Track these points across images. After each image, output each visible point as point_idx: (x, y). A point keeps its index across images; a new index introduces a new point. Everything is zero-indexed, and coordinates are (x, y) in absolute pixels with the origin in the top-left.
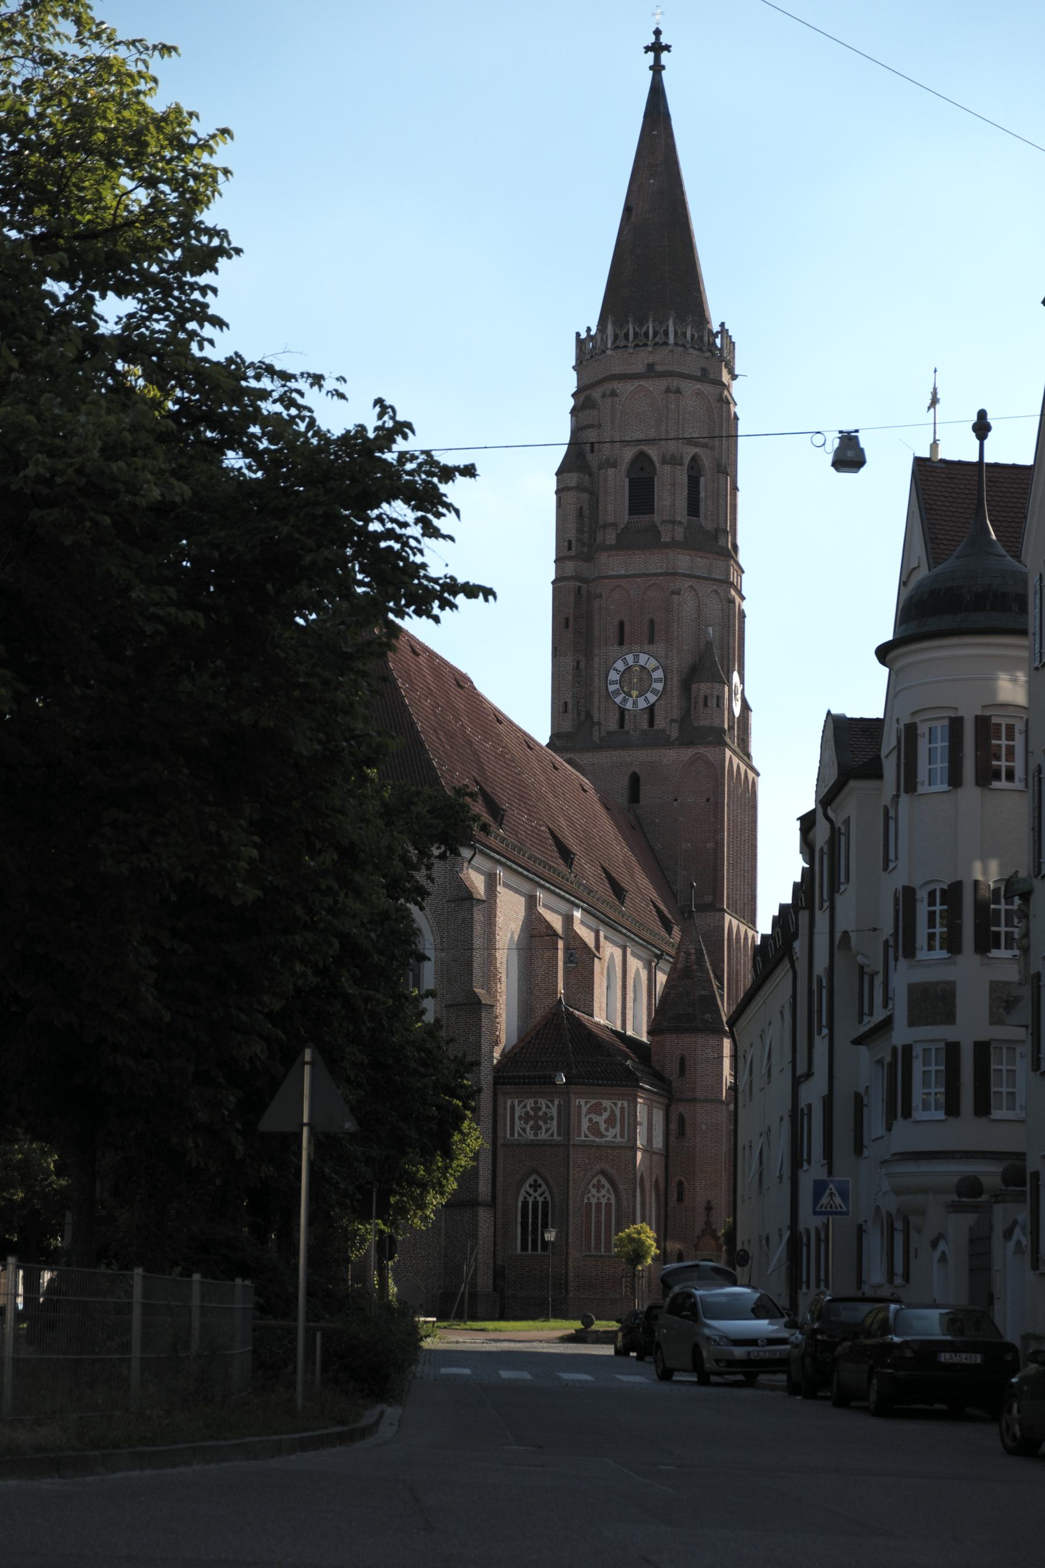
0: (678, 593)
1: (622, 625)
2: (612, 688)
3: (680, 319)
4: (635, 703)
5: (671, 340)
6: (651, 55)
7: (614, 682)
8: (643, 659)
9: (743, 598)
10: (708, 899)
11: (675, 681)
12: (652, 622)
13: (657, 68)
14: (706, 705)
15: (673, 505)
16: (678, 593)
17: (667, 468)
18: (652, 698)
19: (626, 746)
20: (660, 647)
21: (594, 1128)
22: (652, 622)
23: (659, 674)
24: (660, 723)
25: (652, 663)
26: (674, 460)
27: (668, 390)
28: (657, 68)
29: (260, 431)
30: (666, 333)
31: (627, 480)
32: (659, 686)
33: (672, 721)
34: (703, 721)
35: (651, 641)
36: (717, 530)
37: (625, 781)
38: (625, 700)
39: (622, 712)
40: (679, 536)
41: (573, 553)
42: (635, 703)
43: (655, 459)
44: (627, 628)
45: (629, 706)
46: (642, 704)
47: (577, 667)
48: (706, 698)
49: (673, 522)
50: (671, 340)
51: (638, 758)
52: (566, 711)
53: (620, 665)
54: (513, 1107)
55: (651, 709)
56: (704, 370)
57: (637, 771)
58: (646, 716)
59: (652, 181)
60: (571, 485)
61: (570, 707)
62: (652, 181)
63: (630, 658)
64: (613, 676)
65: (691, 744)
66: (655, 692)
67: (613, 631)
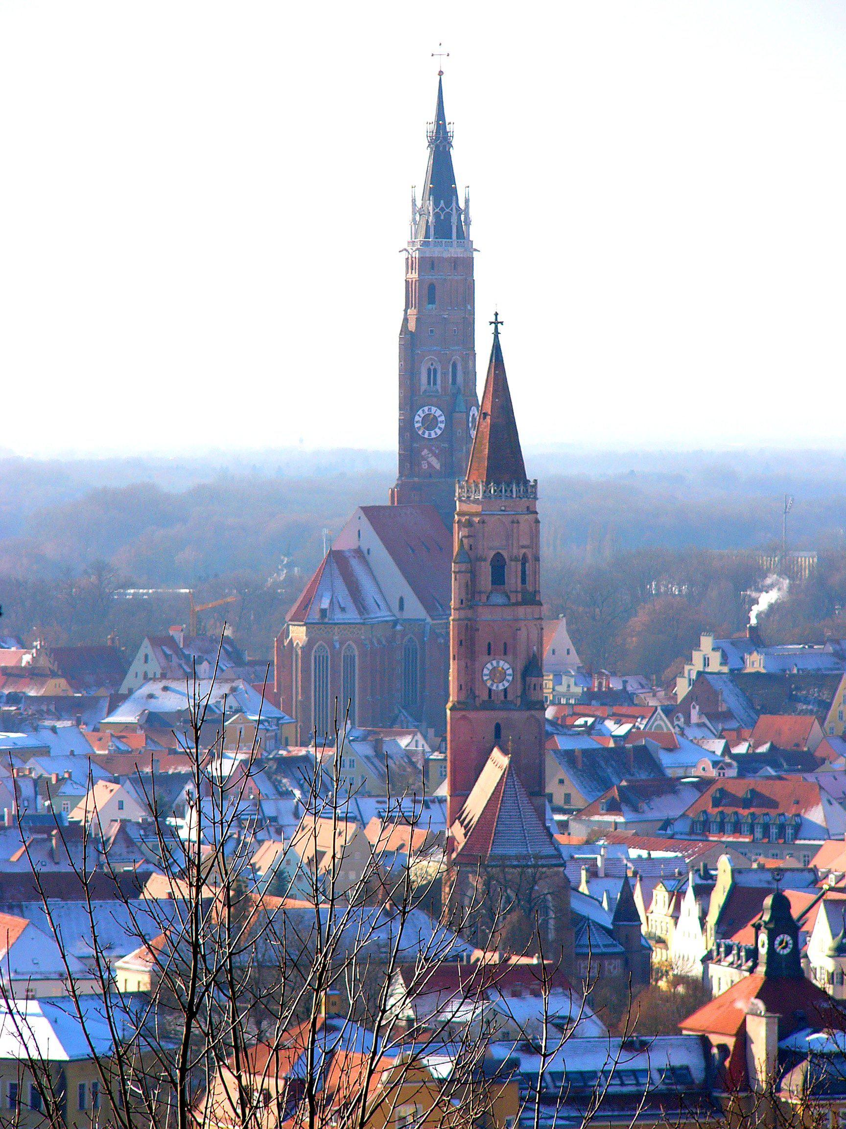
0: (520, 630)
1: (489, 644)
2: (485, 678)
3: (518, 484)
4: (497, 687)
5: (514, 496)
6: (493, 325)
7: (486, 675)
8: (502, 663)
9: (393, 491)
10: (537, 788)
11: (519, 676)
12: (505, 644)
13: (496, 334)
14: (535, 689)
15: (516, 582)
16: (520, 630)
17: (513, 563)
18: (506, 684)
19: (494, 709)
20: (510, 657)
21: (609, 970)
22: (505, 644)
23: (510, 672)
24: (510, 697)
25: (506, 666)
26: (516, 559)
27: (513, 522)
28: (496, 334)
29: (546, 726)
30: (511, 491)
31: (490, 567)
32: (510, 678)
33: (517, 697)
34: (534, 696)
35: (505, 654)
36: (535, 592)
37: (493, 728)
38: (492, 685)
39: (490, 690)
40: (520, 599)
41: (464, 606)
42: (497, 687)
43: (506, 557)
44: (492, 647)
45: (494, 688)
46: (501, 687)
47: (467, 667)
48: (535, 685)
49: (516, 592)
50: (514, 496)
51: (499, 716)
52: (461, 689)
53: (489, 666)
54: (580, 964)
55: (505, 690)
56: (528, 508)
57: (500, 722)
58: (503, 693)
59: (497, 400)
60: (463, 570)
61: (463, 687)
62: (497, 400)
63: (494, 663)
64: (486, 671)
65: (529, 709)
66: (508, 681)
67: (485, 649)
